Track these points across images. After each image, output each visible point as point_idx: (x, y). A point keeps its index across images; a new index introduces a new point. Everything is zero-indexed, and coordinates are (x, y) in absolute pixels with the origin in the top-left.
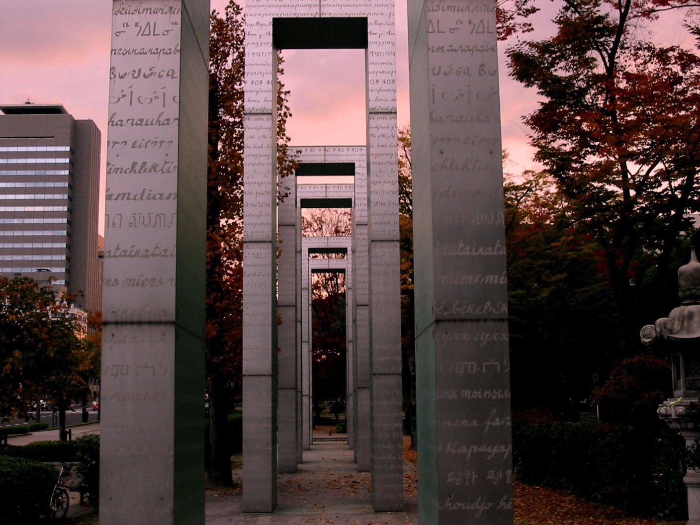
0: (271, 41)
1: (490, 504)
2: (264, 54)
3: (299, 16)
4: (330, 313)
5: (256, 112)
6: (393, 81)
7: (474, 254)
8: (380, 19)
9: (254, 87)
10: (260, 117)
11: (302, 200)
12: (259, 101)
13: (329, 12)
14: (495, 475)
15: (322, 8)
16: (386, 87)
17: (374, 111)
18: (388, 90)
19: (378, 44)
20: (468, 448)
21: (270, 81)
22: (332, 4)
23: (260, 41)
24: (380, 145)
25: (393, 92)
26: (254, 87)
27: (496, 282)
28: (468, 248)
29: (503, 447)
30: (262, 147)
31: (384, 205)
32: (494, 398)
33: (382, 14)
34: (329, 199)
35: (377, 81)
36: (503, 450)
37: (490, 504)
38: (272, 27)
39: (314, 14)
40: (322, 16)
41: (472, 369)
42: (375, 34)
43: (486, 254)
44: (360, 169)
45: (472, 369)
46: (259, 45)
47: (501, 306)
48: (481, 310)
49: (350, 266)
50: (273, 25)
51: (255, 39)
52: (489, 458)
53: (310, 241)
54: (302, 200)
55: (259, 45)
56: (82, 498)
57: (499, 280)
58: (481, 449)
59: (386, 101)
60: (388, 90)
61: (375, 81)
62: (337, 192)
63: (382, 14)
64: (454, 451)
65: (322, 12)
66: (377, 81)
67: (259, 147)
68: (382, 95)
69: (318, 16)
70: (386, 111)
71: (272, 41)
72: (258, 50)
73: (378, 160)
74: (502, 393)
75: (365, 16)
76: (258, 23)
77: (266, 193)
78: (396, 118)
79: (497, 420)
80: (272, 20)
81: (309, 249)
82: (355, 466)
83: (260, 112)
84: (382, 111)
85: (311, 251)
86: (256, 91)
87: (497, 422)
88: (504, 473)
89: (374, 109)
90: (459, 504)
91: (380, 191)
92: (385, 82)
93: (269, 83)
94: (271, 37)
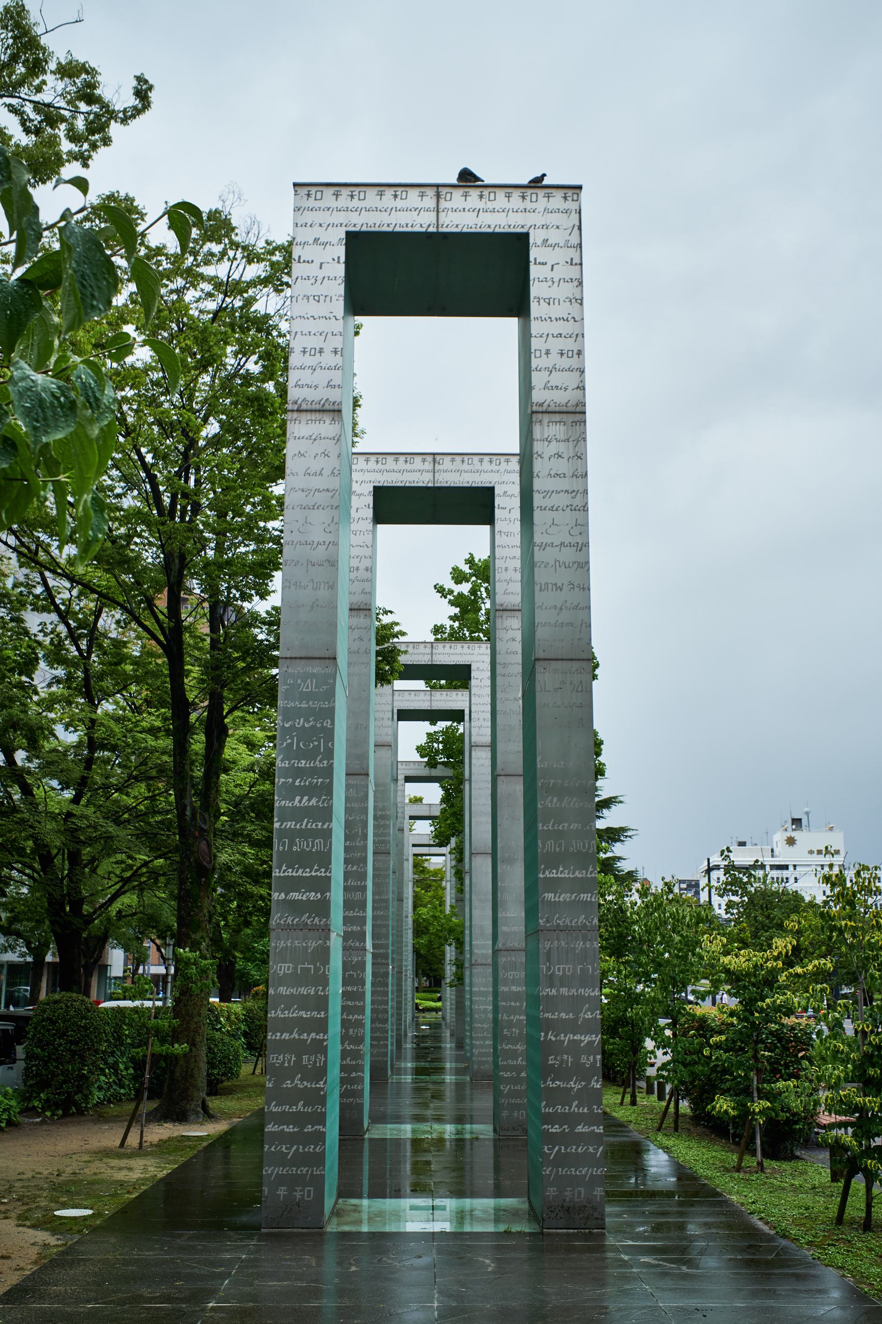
0: (343, 274)
1: (583, 1083)
2: (328, 298)
3: (398, 229)
5: (309, 407)
7: (571, 876)
8: (554, 237)
9: (309, 361)
10: (318, 416)
11: (379, 493)
13: (455, 222)
14: (588, 1059)
15: (442, 215)
16: (565, 362)
17: (540, 409)
18: (570, 370)
19: (550, 283)
20: (565, 1036)
22: (461, 208)
23: (320, 274)
24: (553, 473)
25: (578, 373)
26: (309, 361)
27: (589, 899)
28: (566, 871)
29: (594, 1036)
30: (321, 474)
31: (561, 590)
32: (587, 995)
33: (558, 227)
34: (439, 488)
35: (548, 353)
36: (594, 1039)
37: (583, 1083)
38: (344, 247)
39: (425, 226)
40: (441, 230)
41: (569, 971)
43: (580, 876)
44: (508, 506)
45: (569, 971)
46: (319, 282)
47: (593, 919)
48: (577, 922)
50: (346, 244)
51: (312, 270)
52: (582, 1045)
54: (379, 493)
55: (319, 282)
57: (591, 897)
58: (575, 1038)
59: (566, 389)
60: (570, 370)
61: (543, 352)
63: (558, 227)
64: (553, 1039)
65: (441, 222)
66: (548, 353)
67: (315, 474)
68: (557, 379)
69: (435, 230)
70: (565, 409)
71: (343, 275)
72: (317, 290)
73: (548, 503)
74: (593, 991)
75: (524, 230)
76: (316, 240)
77: (326, 564)
78: (585, 422)
79: (589, 1013)
80: (344, 236)
83: (318, 407)
84: (557, 409)
87: (589, 1016)
88: (594, 1058)
89: (542, 405)
90: (557, 1082)
91: (552, 562)
92: (562, 354)
94: (342, 267)
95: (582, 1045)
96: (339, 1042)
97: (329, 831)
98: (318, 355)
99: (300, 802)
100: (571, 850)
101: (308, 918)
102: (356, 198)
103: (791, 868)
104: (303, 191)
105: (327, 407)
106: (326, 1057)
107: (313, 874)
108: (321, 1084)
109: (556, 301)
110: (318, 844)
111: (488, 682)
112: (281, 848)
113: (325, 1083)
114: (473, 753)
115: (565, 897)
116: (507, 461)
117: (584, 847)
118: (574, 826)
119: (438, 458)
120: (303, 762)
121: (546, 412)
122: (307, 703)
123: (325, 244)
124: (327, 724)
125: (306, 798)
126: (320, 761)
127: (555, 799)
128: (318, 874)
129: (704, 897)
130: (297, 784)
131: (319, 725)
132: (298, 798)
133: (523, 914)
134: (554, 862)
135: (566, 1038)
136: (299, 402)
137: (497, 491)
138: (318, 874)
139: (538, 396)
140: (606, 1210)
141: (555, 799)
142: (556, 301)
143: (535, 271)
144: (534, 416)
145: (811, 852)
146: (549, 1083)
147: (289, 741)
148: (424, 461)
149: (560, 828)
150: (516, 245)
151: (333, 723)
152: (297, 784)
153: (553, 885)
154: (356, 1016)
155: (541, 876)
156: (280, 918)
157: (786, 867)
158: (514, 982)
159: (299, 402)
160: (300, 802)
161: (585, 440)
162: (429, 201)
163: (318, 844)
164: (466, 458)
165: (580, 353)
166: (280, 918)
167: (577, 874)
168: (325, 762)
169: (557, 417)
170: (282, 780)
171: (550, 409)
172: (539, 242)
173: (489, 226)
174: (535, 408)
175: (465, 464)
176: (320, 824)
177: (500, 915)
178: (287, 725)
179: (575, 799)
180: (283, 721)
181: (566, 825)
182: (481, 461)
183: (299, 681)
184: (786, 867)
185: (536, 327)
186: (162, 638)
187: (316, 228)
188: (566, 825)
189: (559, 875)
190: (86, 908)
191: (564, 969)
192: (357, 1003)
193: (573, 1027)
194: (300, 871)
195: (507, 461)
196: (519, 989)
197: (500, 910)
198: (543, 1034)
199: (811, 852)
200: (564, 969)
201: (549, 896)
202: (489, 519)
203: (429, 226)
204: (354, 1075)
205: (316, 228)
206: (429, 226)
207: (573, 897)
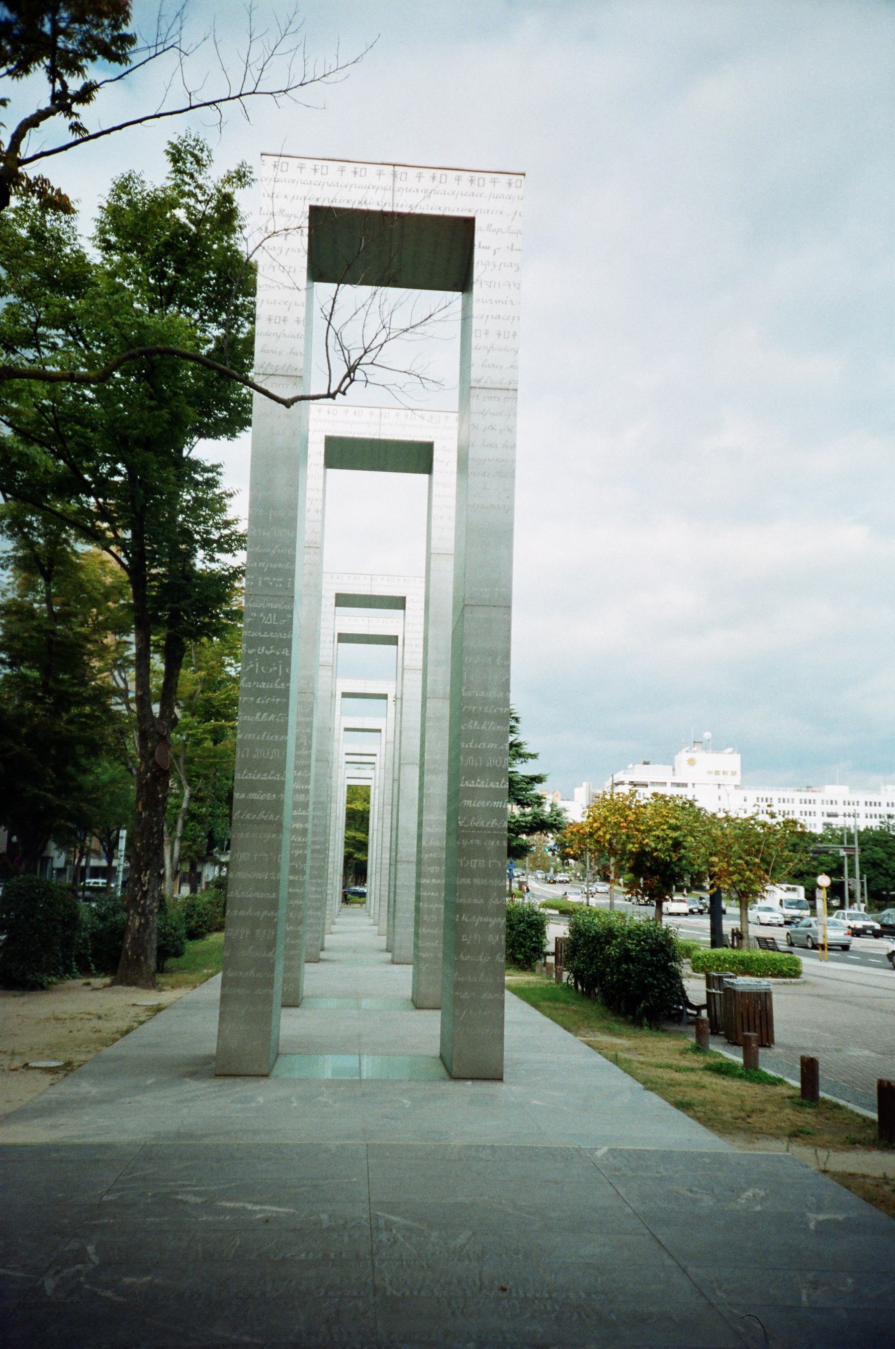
4: (358, 794)
6: (514, 335)
12: (280, 353)
15: (397, 194)
21: (302, 319)
42: (488, 248)
44: (444, 460)
46: (284, 253)
49: (383, 750)
53: (318, 177)
54: (340, 635)
55: (284, 253)
56: (743, 917)
62: (428, 194)
64: (466, 920)
78: (516, 398)
81: (320, 217)
82: (389, 956)
85: (345, 695)
86: (276, 334)
89: (479, 381)
93: (298, 322)
95: (490, 926)
97: (285, 743)
98: (282, 323)
99: (260, 717)
100: (487, 765)
101: (265, 815)
102: (319, 172)
103: (690, 786)
105: (290, 373)
106: (276, 931)
107: (270, 778)
108: (271, 954)
109: (497, 285)
111: (422, 613)
112: (243, 756)
113: (274, 953)
114: (405, 676)
115: (482, 804)
117: (498, 763)
118: (491, 746)
120: (264, 684)
121: (483, 388)
122: (269, 634)
124: (285, 652)
125: (266, 714)
126: (279, 684)
127: (476, 723)
128: (274, 778)
130: (258, 702)
131: (278, 653)
132: (259, 714)
133: (445, 818)
134: (472, 774)
135: (478, 920)
136: (265, 366)
138: (274, 778)
139: (476, 372)
140: (507, 978)
141: (476, 723)
142: (497, 285)
144: (473, 391)
145: (710, 773)
146: (462, 956)
147: (252, 666)
149: (479, 746)
150: (464, 228)
151: (290, 652)
152: (258, 702)
153: (472, 793)
154: (296, 901)
155: (462, 785)
156: (240, 815)
157: (685, 785)
158: (432, 876)
159: (265, 366)
160: (260, 717)
161: (515, 415)
162: (386, 179)
166: (240, 815)
167: (492, 785)
168: (283, 684)
169: (492, 393)
170: (245, 698)
171: (486, 386)
173: (440, 208)
174: (473, 384)
176: (277, 737)
177: (424, 818)
178: (250, 652)
179: (492, 723)
180: (247, 649)
181: (484, 744)
183: (262, 615)
184: (685, 785)
185: (477, 308)
186: (126, 562)
188: (484, 744)
189: (477, 786)
190: (608, 797)
191: (477, 863)
192: (297, 890)
193: (483, 912)
194: (259, 776)
196: (439, 881)
197: (425, 813)
198: (458, 916)
199: (710, 773)
200: (477, 863)
201: (468, 803)
202: (428, 469)
203: (385, 204)
204: (292, 952)
206: (385, 204)
207: (488, 804)
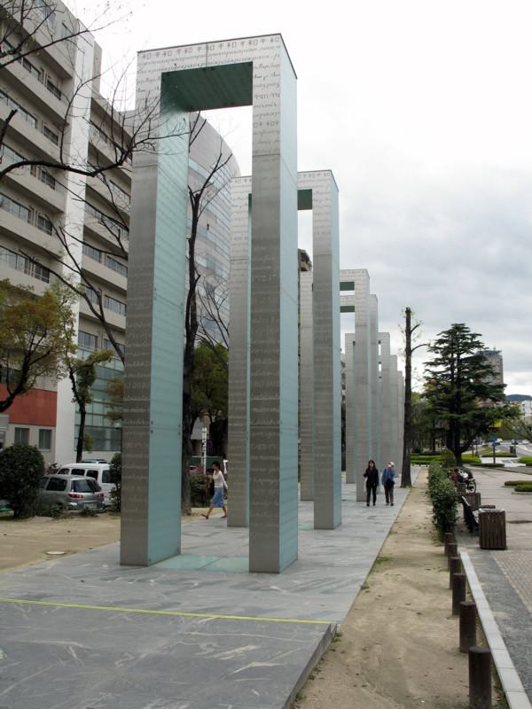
34: (213, 68)
76: (147, 79)
96: (75, 555)
104: (142, 55)
110: (243, 408)
116: (263, 41)
119: (209, 45)
123: (151, 81)
129: (489, 400)
137: (254, 65)
143: (255, 82)
148: (199, 49)
163: (243, 408)
164: (231, 42)
165: (277, 123)
172: (257, 66)
175: (231, 47)
182: (243, 43)
187: (147, 73)
195: (263, 41)
205: (147, 73)
